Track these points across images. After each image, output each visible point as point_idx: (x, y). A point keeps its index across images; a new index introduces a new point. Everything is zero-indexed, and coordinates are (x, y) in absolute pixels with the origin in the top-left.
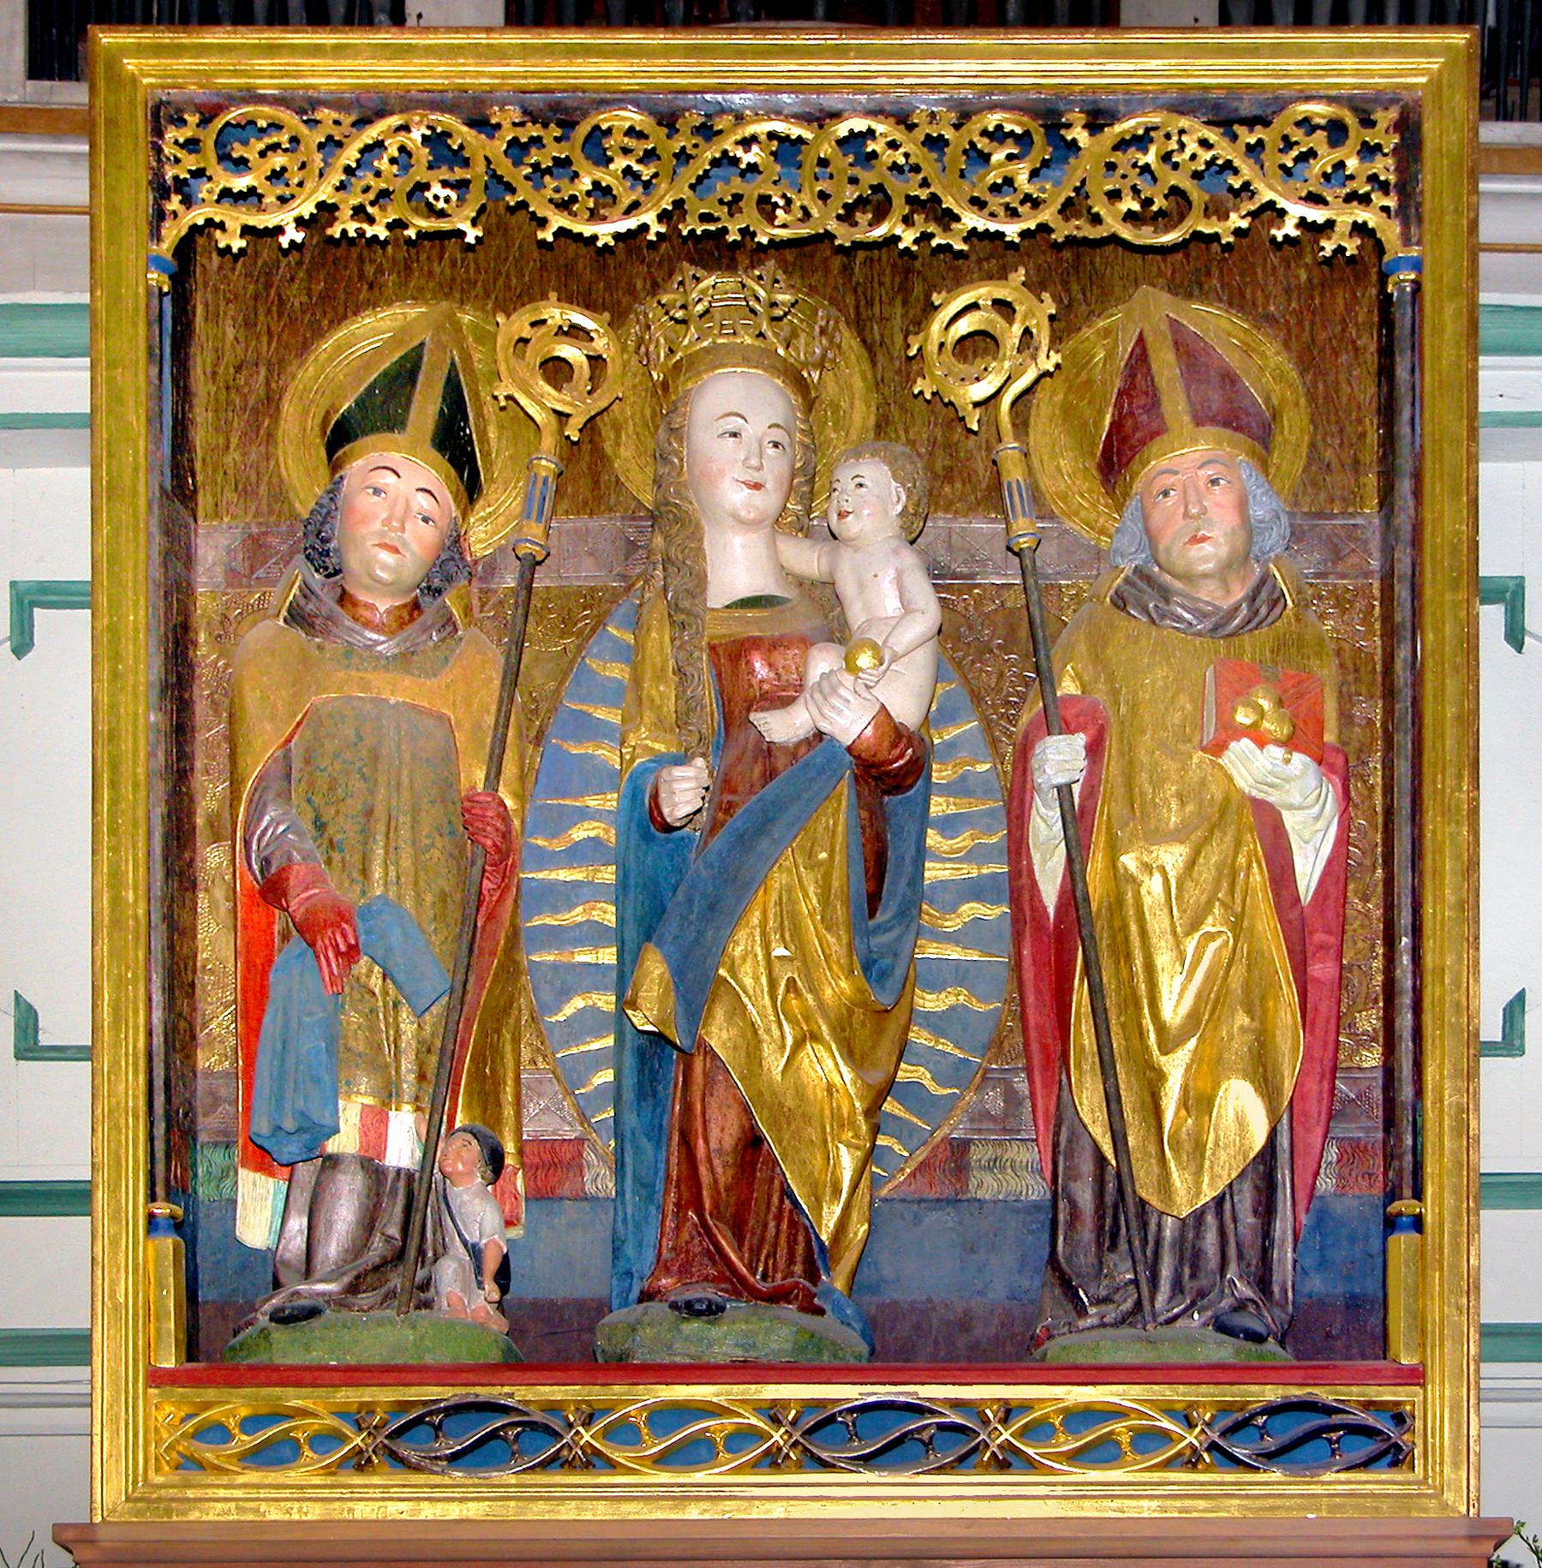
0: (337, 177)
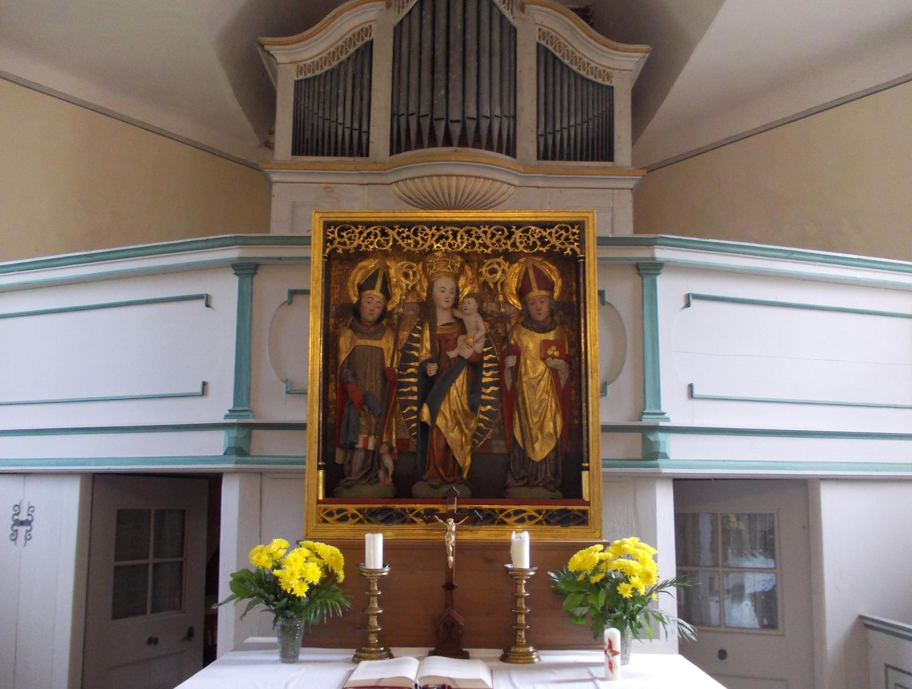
0: (362, 239)
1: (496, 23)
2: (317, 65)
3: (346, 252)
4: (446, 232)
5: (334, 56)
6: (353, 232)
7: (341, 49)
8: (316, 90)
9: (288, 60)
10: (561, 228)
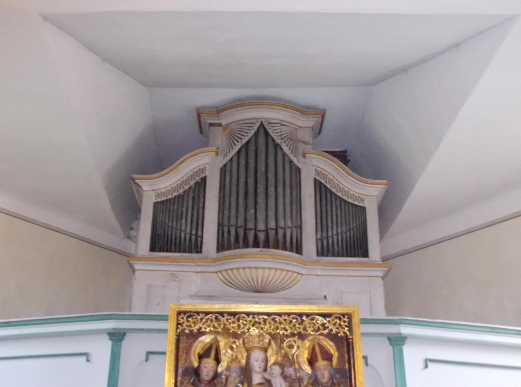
0: (202, 323)
1: (287, 166)
2: (169, 192)
3: (191, 331)
4: (259, 319)
5: (180, 186)
6: (197, 318)
7: (186, 182)
8: (168, 208)
9: (150, 189)
10: (336, 318)
